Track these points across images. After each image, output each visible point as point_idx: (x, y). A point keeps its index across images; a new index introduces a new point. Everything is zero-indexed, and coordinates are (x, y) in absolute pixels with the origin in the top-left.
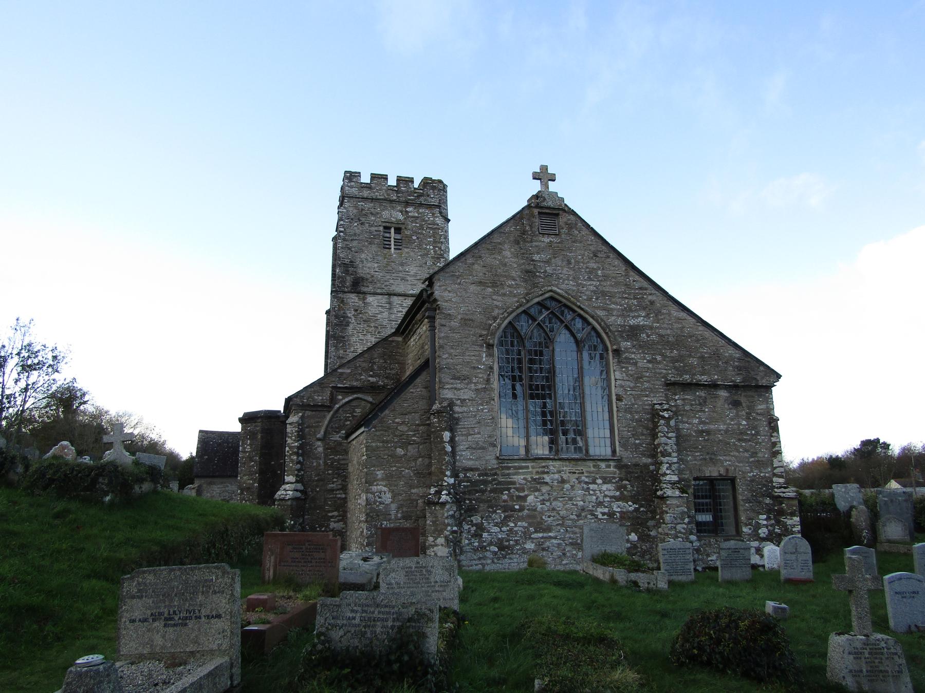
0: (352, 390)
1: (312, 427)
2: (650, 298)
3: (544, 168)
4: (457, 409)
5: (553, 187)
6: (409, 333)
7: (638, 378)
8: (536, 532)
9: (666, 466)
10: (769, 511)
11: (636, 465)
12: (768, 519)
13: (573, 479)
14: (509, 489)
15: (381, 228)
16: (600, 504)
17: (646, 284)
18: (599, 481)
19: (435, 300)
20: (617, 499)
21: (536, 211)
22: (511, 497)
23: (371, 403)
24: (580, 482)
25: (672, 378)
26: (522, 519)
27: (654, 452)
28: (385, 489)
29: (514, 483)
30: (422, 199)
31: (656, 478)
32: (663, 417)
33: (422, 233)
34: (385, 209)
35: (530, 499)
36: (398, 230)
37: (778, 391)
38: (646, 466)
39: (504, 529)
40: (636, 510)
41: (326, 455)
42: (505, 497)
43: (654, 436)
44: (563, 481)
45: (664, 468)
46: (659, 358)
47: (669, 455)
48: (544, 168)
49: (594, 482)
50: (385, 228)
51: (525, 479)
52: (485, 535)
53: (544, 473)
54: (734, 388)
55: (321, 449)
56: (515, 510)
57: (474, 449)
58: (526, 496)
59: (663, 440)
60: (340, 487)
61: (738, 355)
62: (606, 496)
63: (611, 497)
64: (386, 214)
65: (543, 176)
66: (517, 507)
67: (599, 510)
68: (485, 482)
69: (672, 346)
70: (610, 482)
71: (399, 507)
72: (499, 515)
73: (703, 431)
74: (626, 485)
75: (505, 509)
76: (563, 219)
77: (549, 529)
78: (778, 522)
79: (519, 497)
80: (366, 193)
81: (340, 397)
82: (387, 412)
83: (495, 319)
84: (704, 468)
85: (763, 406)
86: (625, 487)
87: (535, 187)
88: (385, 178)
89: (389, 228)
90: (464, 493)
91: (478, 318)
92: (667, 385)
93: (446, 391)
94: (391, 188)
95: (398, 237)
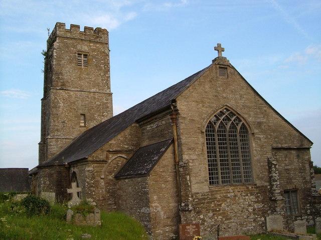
0: (116, 152)
1: (98, 172)
2: (264, 108)
3: (219, 45)
4: (190, 164)
5: (224, 54)
6: (149, 122)
7: (262, 147)
8: (226, 220)
9: (275, 186)
10: (310, 203)
11: (263, 186)
12: (310, 206)
13: (239, 194)
14: (214, 201)
15: (77, 55)
16: (250, 205)
17: (263, 102)
18: (249, 195)
19: (177, 110)
20: (256, 202)
21: (218, 66)
22: (215, 205)
23: (126, 159)
24: (242, 196)
25: (275, 145)
26: (220, 215)
27: (271, 179)
28: (158, 205)
29: (216, 198)
30: (98, 40)
31: (271, 192)
32: (273, 164)
33: (98, 58)
34: (79, 43)
35: (223, 205)
36: (85, 56)
37: (312, 150)
38: (266, 186)
39: (213, 220)
40: (264, 206)
41: (106, 187)
42: (213, 205)
43: (270, 172)
44: (235, 196)
45: (275, 187)
46: (269, 137)
47: (276, 181)
48: (219, 45)
49: (247, 195)
50: (78, 54)
51: (220, 196)
52: (205, 224)
53: (227, 192)
54: (298, 149)
55: (103, 184)
56: (217, 211)
57: (199, 183)
58: (221, 204)
59: (274, 174)
60: (113, 202)
61: (297, 134)
62: (252, 201)
63: (254, 202)
64: (79, 47)
65: (219, 49)
66: (218, 209)
67: (250, 208)
68: (204, 199)
69: (274, 131)
70: (253, 195)
71: (165, 213)
72: (211, 214)
73: (286, 169)
74: (259, 196)
75: (214, 211)
76: (229, 70)
77: (231, 219)
78: (314, 207)
79: (219, 205)
80: (69, 35)
81: (111, 156)
82: (156, 166)
83: (204, 119)
84: (288, 186)
85: (307, 157)
86: (258, 197)
87: (215, 55)
88: (78, 27)
89: (81, 55)
90: (196, 205)
91: (196, 119)
92: (273, 149)
93: (185, 156)
94: (81, 33)
95: (86, 59)
